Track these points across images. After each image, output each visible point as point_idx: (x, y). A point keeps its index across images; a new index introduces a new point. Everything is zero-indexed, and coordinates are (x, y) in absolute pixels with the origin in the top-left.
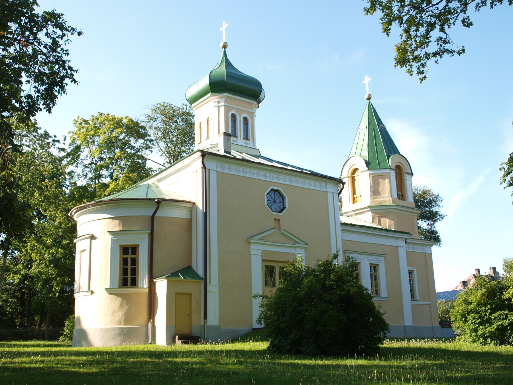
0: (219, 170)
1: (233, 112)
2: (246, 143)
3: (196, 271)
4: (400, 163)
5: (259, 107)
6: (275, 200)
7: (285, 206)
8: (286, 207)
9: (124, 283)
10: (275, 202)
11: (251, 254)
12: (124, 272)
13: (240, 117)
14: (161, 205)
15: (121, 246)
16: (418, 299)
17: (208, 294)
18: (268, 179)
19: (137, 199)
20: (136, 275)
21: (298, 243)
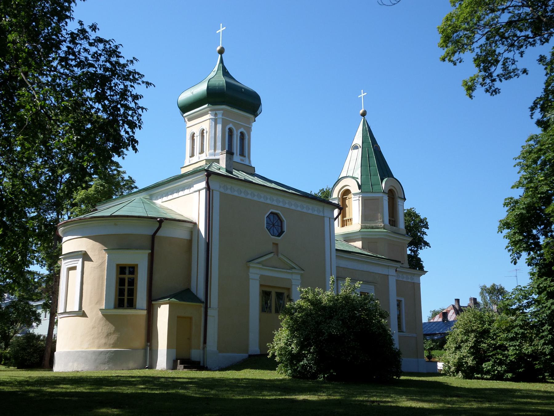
0: (222, 190)
1: (231, 126)
2: (241, 160)
3: (196, 294)
4: (394, 187)
5: (255, 121)
6: (274, 222)
7: (283, 231)
8: (284, 231)
9: (120, 304)
10: (274, 225)
11: (292, 285)
12: (121, 292)
13: (237, 132)
14: (163, 224)
15: (117, 265)
16: (404, 331)
17: (208, 317)
18: (268, 202)
19: (139, 217)
20: (133, 296)
21: (295, 268)
